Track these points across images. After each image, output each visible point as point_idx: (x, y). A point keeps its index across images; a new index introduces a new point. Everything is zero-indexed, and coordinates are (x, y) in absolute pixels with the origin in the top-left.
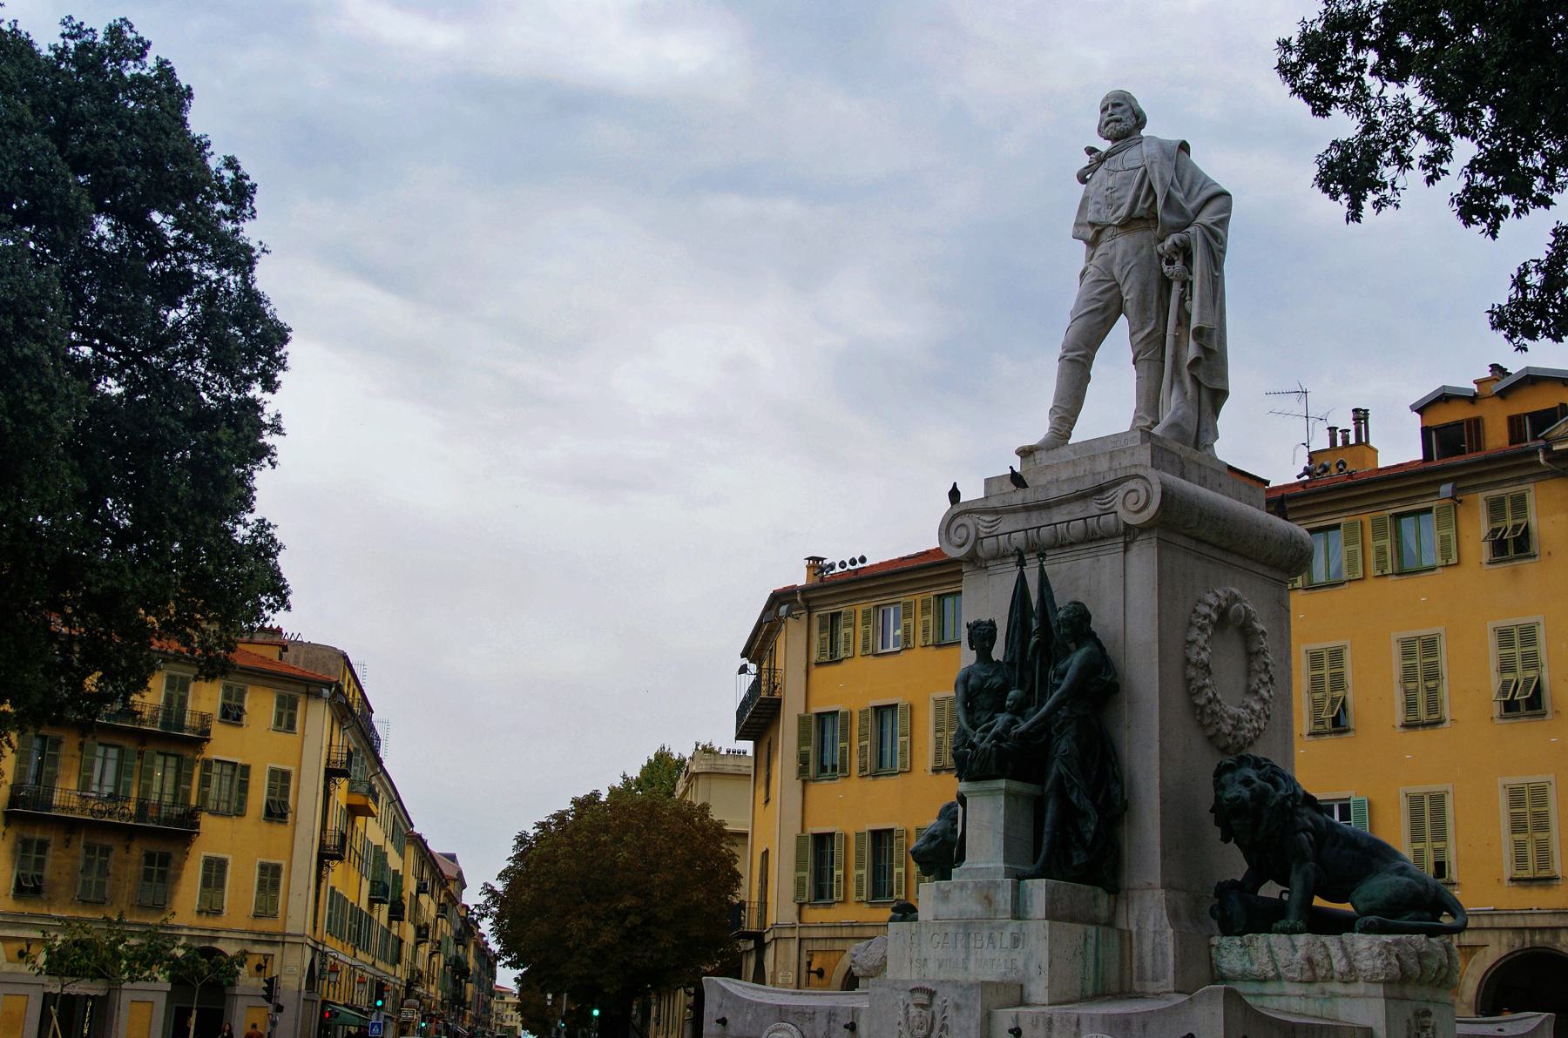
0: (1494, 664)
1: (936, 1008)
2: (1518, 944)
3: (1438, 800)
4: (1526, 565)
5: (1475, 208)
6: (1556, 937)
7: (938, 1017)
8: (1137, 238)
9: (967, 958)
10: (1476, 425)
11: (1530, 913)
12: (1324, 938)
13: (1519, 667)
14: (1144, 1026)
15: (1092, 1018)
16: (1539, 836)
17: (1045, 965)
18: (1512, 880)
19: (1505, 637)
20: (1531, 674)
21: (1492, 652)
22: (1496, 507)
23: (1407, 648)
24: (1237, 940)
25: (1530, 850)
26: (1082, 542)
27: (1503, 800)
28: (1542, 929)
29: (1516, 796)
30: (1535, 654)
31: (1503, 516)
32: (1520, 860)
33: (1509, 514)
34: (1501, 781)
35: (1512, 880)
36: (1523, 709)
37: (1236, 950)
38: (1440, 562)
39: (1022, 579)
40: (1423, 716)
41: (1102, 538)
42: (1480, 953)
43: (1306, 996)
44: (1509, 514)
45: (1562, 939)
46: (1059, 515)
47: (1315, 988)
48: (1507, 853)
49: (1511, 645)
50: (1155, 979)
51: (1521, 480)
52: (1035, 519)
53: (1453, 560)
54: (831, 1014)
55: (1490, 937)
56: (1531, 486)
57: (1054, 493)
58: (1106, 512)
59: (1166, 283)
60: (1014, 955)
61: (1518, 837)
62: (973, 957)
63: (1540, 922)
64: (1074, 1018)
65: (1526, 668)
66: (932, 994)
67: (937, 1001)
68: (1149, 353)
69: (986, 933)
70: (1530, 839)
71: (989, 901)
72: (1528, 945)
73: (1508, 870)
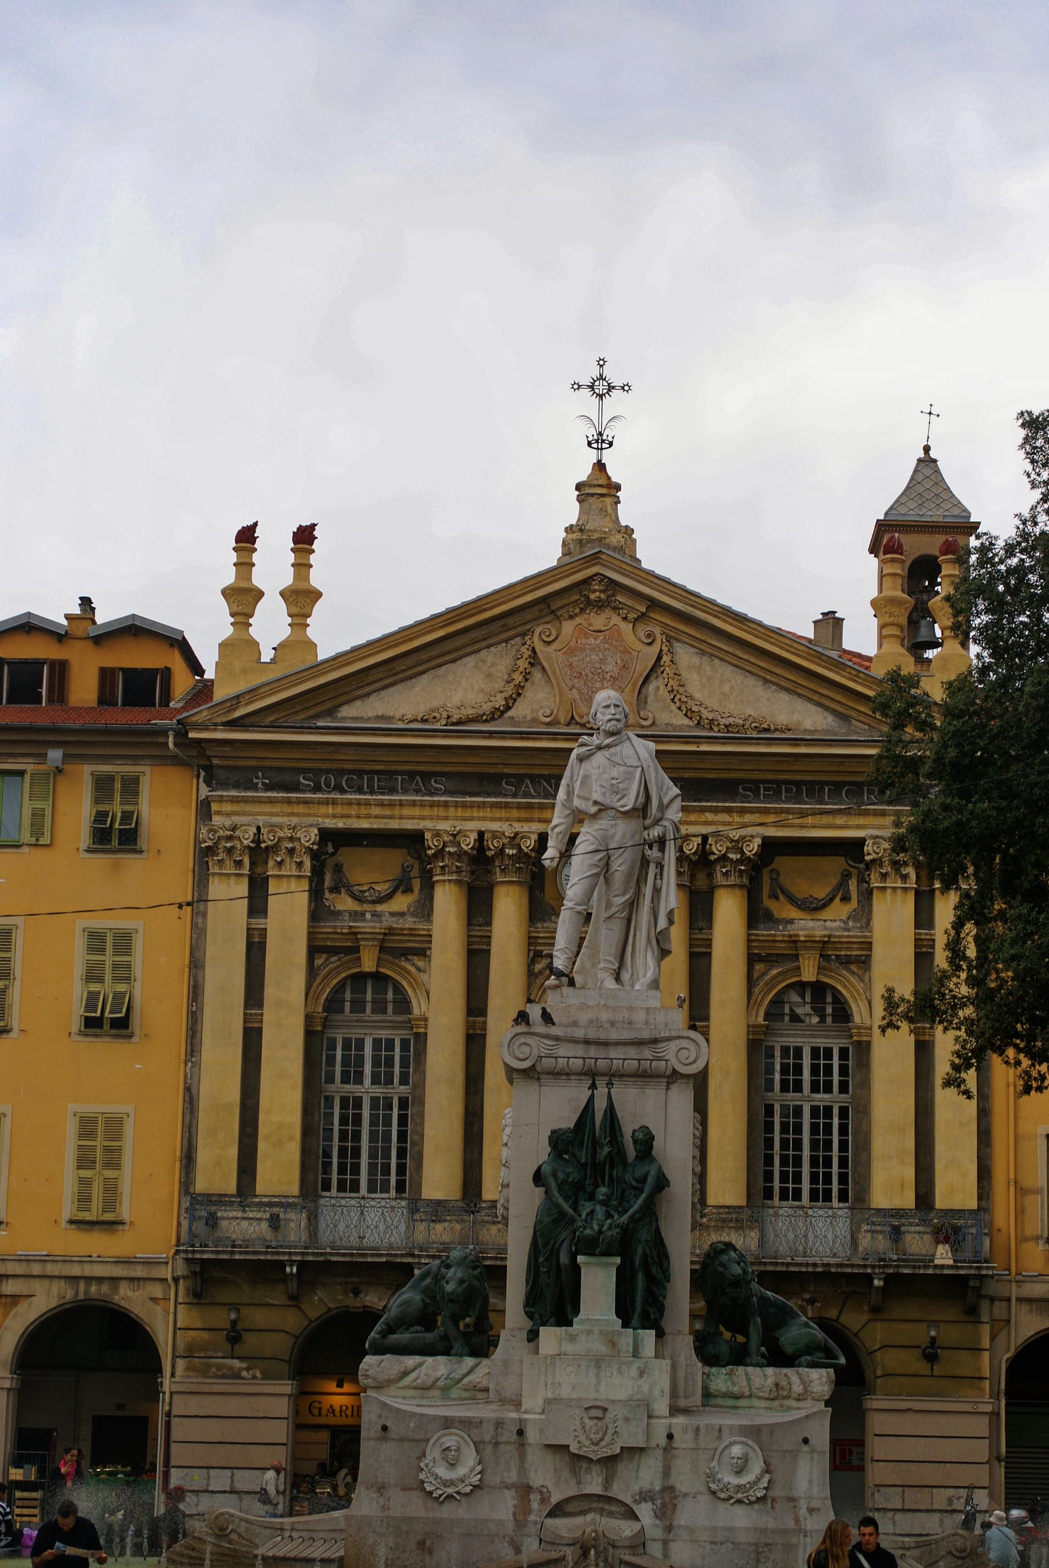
0: (79, 970)
1: (607, 1420)
2: (69, 1295)
6: (115, 1289)
7: (611, 1426)
8: (635, 824)
9: (599, 1384)
10: (60, 670)
11: (87, 1260)
12: (785, 1370)
13: (108, 978)
14: (771, 1432)
15: (731, 1427)
16: (109, 1173)
17: (667, 1391)
18: (71, 1222)
20: (121, 988)
21: (79, 958)
22: (103, 786)
24: (723, 1370)
25: (97, 1191)
26: (630, 1076)
27: (72, 1129)
28: (100, 1280)
29: (87, 1126)
30: (128, 966)
31: (111, 798)
32: (84, 1199)
33: (117, 796)
34: (72, 1107)
35: (71, 1222)
36: (107, 1026)
37: (722, 1377)
38: (26, 837)
39: (591, 1099)
41: (650, 1076)
42: (22, 1307)
43: (770, 1409)
44: (117, 796)
45: (122, 1291)
46: (615, 1053)
47: (776, 1403)
48: (69, 1189)
49: (102, 951)
50: (686, 1397)
51: (136, 759)
52: (593, 1051)
53: (45, 840)
54: (499, 1424)
55: (38, 1287)
56: (147, 769)
57: (614, 1035)
58: (659, 1059)
59: (645, 862)
60: (640, 1382)
61: (84, 1173)
62: (603, 1383)
63: (99, 1271)
64: (717, 1428)
65: (116, 979)
66: (605, 1410)
67: (609, 1415)
69: (616, 1367)
70: (97, 1176)
71: (613, 1344)
72: (81, 1297)
73: (68, 1210)
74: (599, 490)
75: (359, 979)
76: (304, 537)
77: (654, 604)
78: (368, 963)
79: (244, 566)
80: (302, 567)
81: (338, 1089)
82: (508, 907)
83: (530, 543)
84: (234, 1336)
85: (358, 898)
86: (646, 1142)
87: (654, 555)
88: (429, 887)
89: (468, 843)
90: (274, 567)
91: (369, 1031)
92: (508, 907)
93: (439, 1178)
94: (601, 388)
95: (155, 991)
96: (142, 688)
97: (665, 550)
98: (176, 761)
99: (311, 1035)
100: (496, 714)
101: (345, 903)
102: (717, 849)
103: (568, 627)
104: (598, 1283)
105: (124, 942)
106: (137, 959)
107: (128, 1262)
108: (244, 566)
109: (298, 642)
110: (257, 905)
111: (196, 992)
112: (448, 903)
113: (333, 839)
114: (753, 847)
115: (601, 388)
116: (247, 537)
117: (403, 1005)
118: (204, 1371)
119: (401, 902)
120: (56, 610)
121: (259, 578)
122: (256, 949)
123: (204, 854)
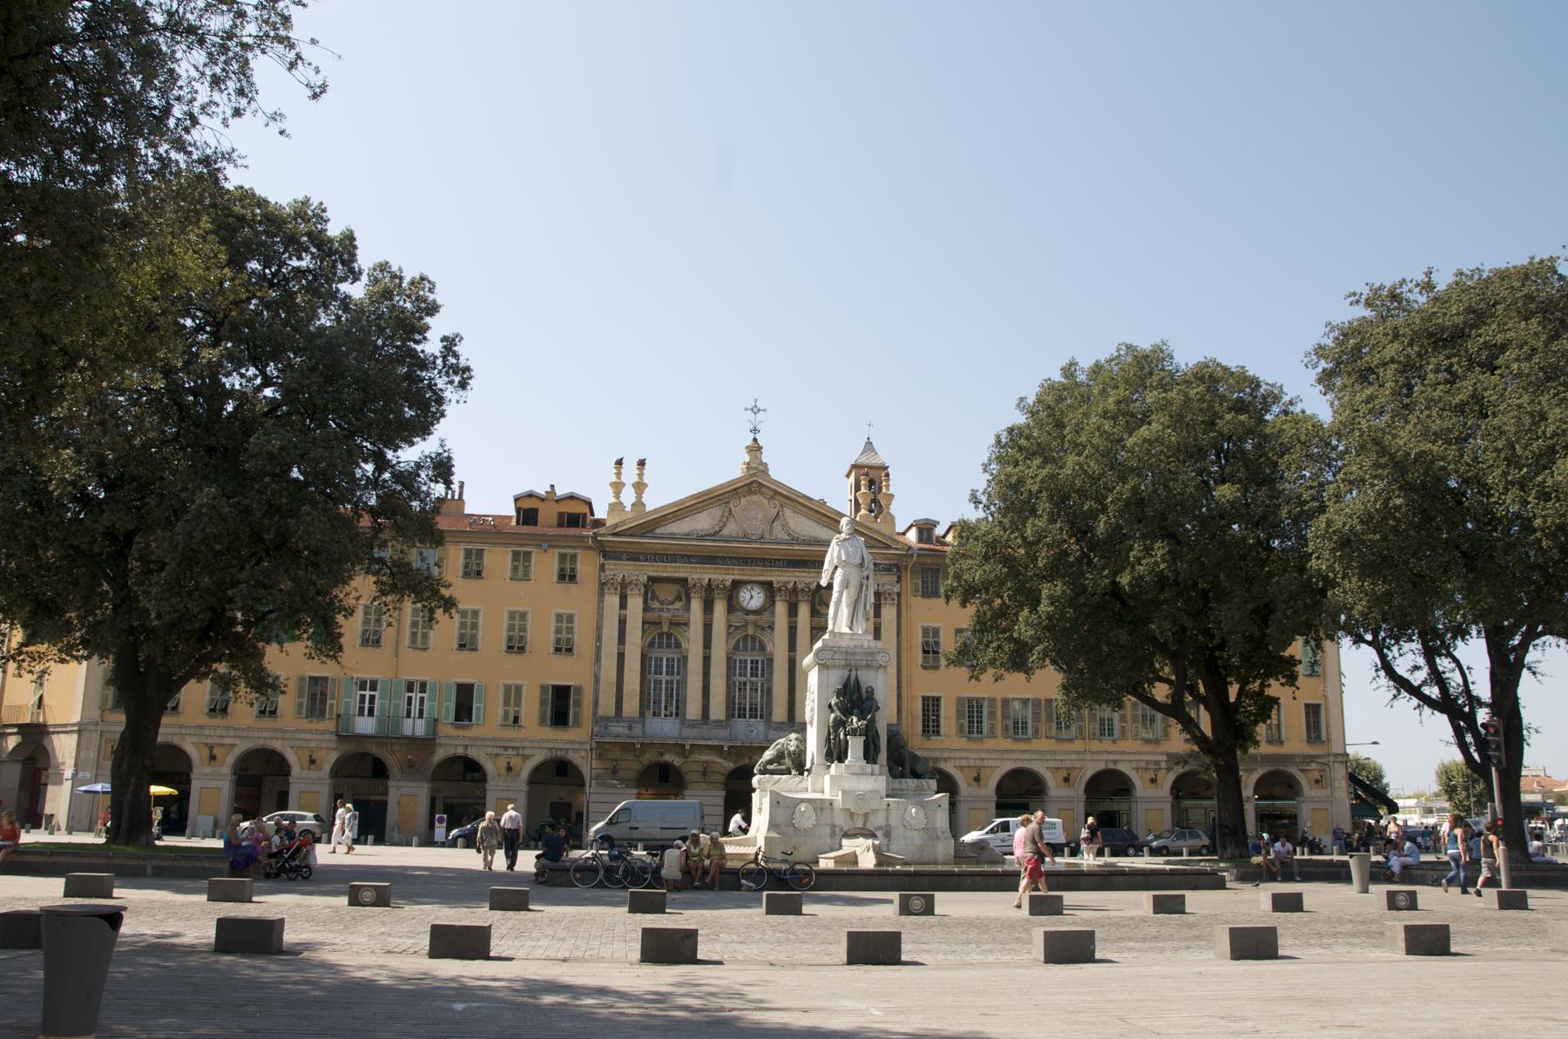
0: (553, 630)
3: (519, 688)
4: (572, 585)
5: (964, 605)
19: (559, 618)
23: (512, 615)
40: (516, 646)
68: (1309, 764)
74: (755, 449)
75: (661, 635)
76: (642, 463)
77: (776, 492)
78: (665, 628)
79: (619, 474)
80: (641, 475)
81: (653, 677)
82: (804, 611)
83: (731, 469)
84: (614, 772)
85: (661, 602)
86: (871, 692)
87: (775, 474)
88: (689, 599)
89: (790, 586)
90: (630, 474)
91: (666, 654)
92: (804, 611)
93: (693, 710)
94: (755, 410)
95: (582, 636)
96: (574, 520)
97: (782, 471)
98: (592, 549)
99: (643, 656)
100: (716, 533)
101: (656, 605)
102: (800, 586)
103: (743, 500)
104: (856, 746)
105: (570, 618)
106: (576, 626)
107: (573, 742)
108: (619, 474)
109: (639, 504)
110: (623, 605)
111: (599, 638)
112: (696, 606)
113: (653, 580)
114: (728, 583)
115: (755, 410)
116: (619, 463)
117: (678, 645)
118: (603, 785)
119: (678, 605)
120: (542, 490)
121: (623, 479)
122: (622, 623)
123: (602, 585)
